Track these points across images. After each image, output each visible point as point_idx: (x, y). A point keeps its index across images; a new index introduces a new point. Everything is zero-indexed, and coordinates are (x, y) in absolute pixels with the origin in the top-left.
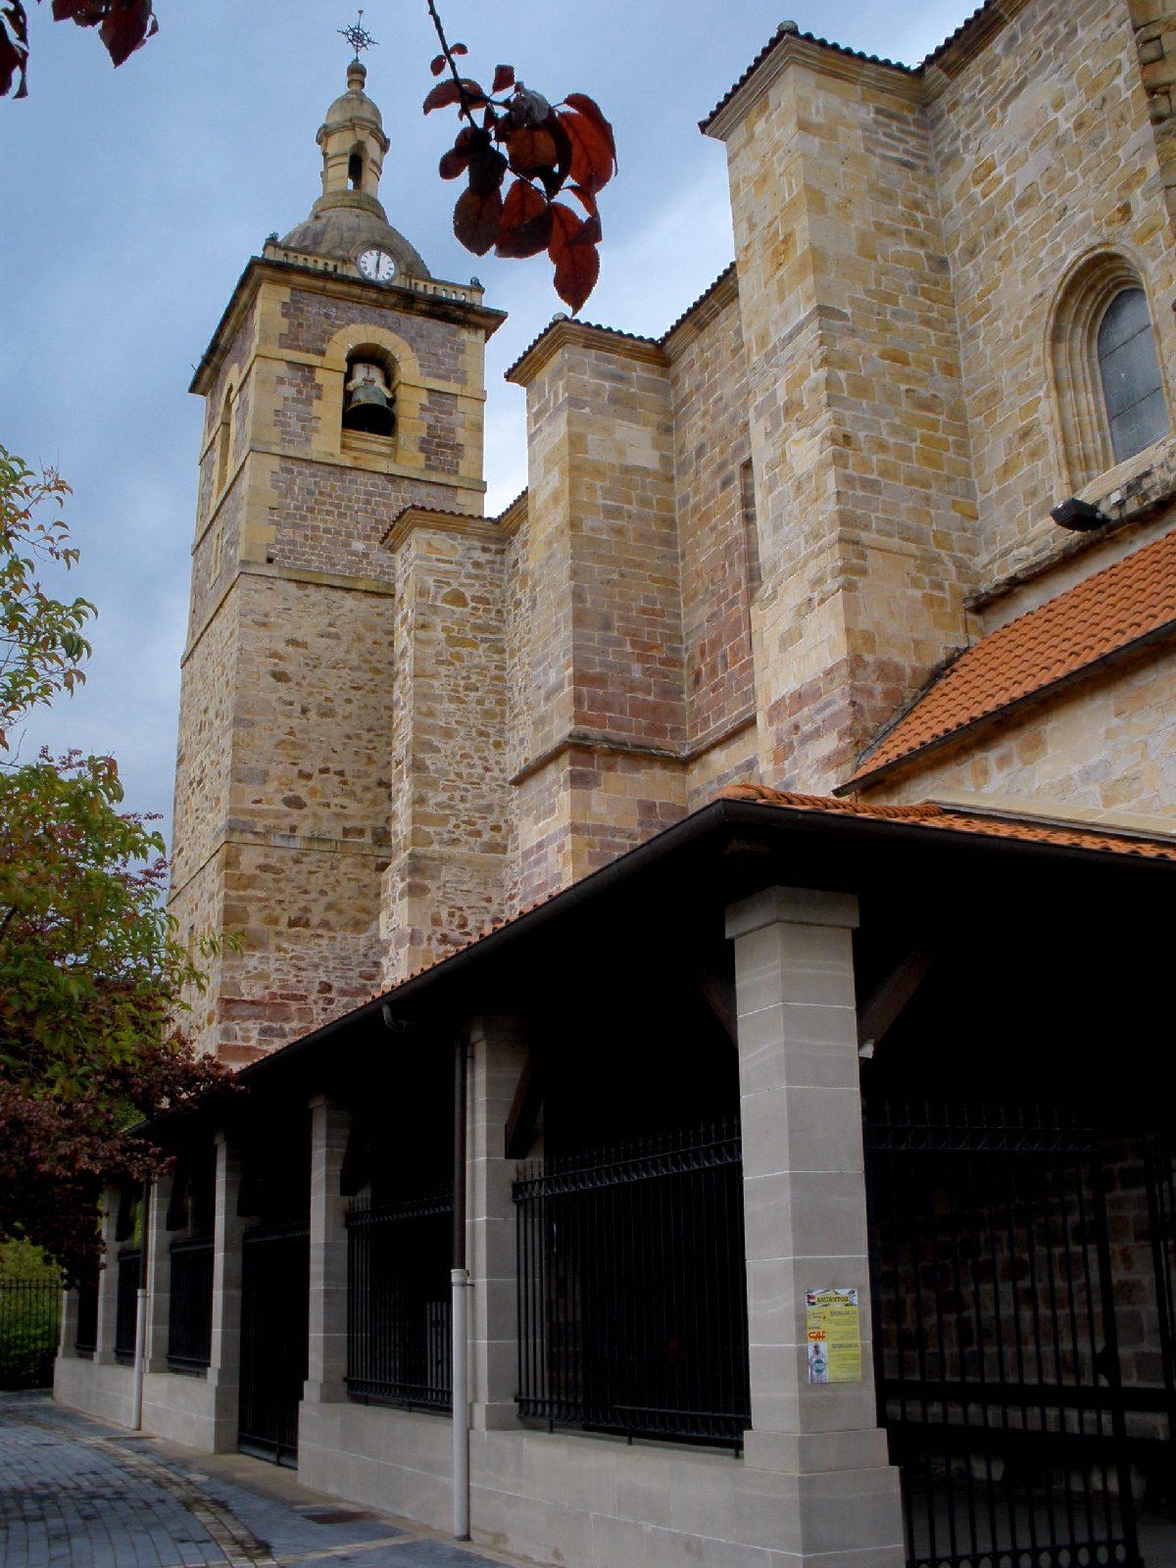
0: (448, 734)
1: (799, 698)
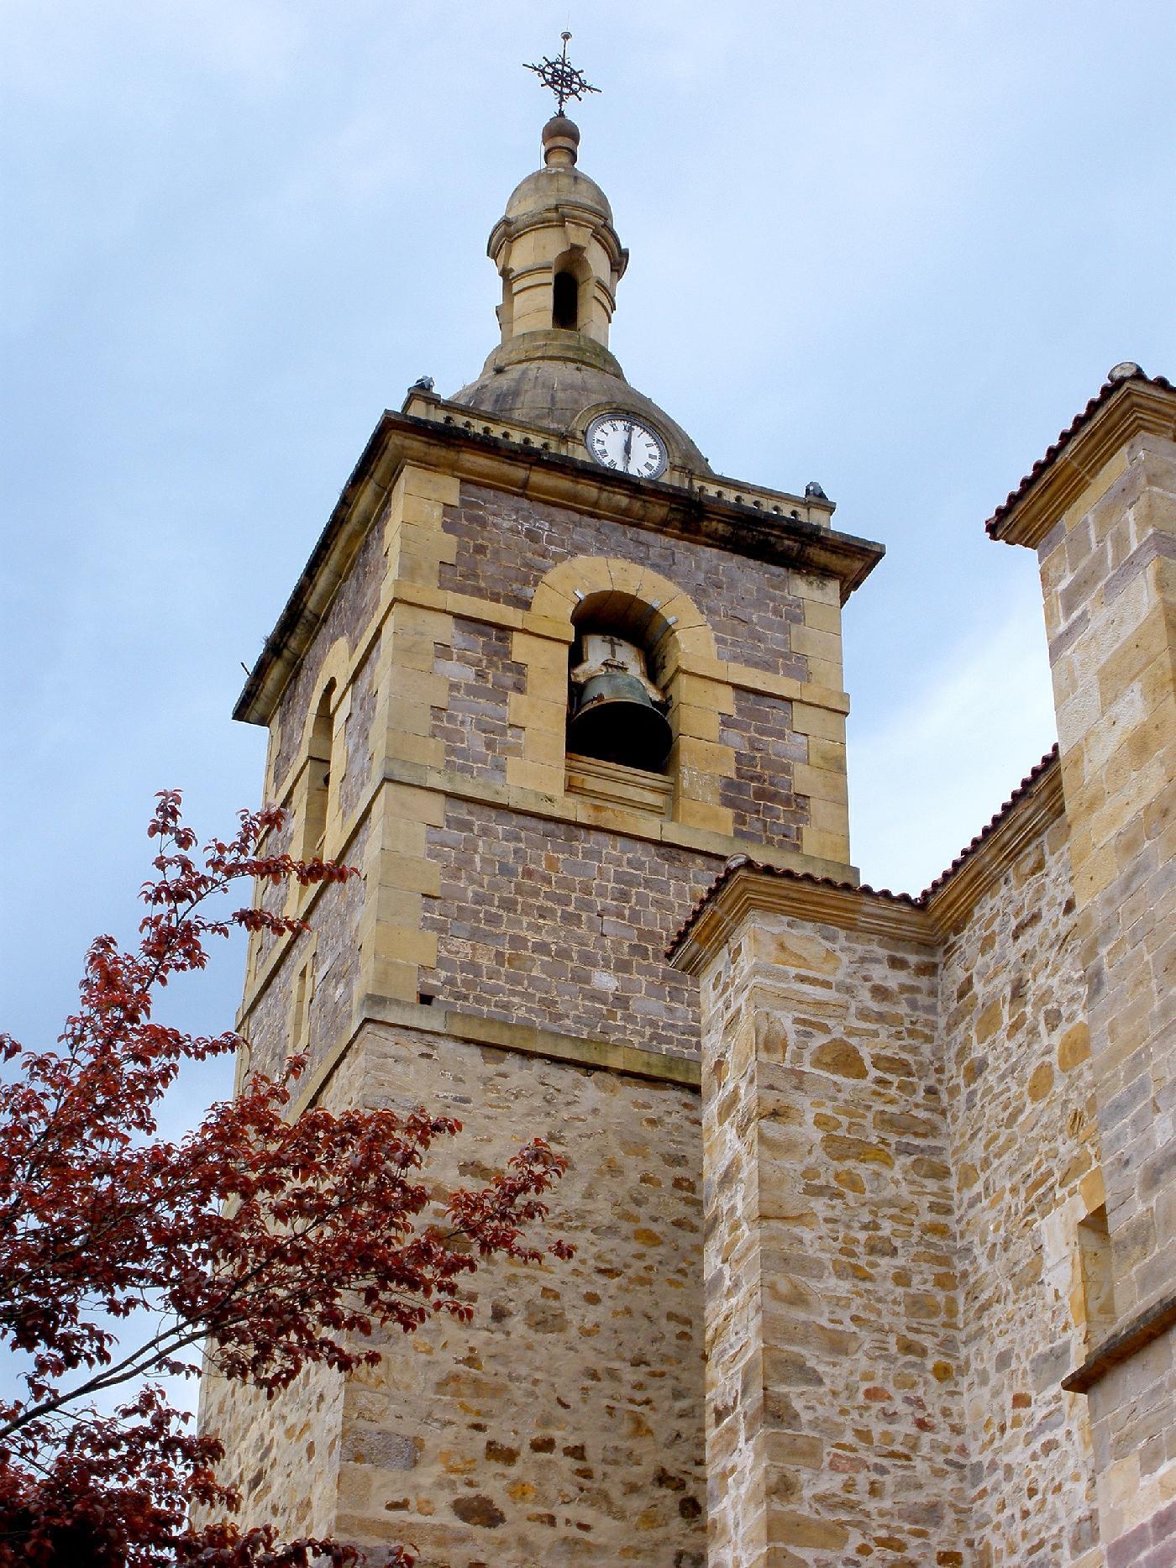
0: (838, 1345)
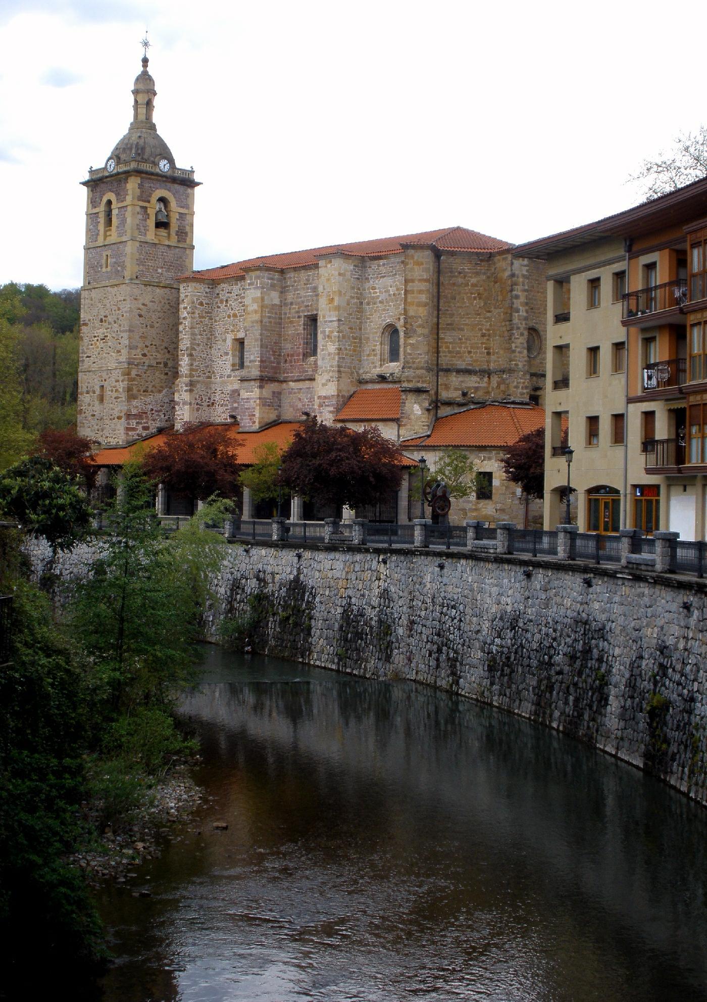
1: (325, 397)
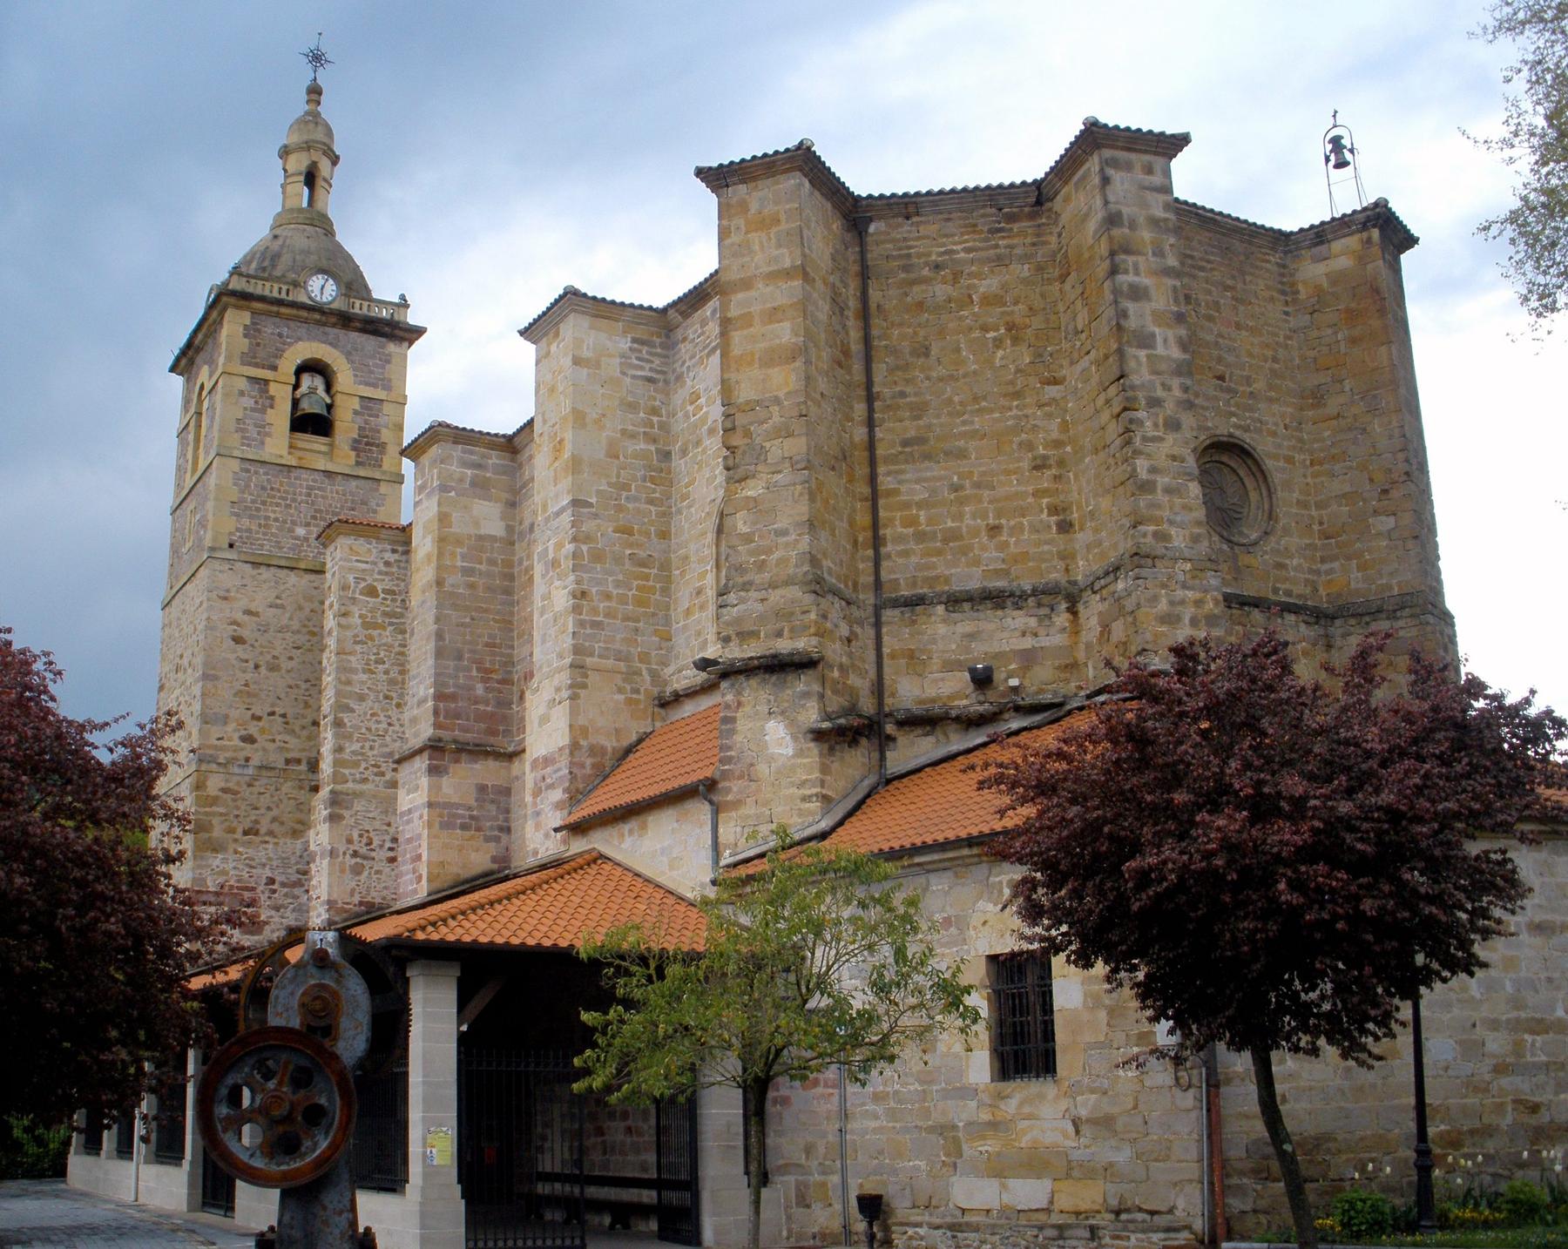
0: (361, 698)
